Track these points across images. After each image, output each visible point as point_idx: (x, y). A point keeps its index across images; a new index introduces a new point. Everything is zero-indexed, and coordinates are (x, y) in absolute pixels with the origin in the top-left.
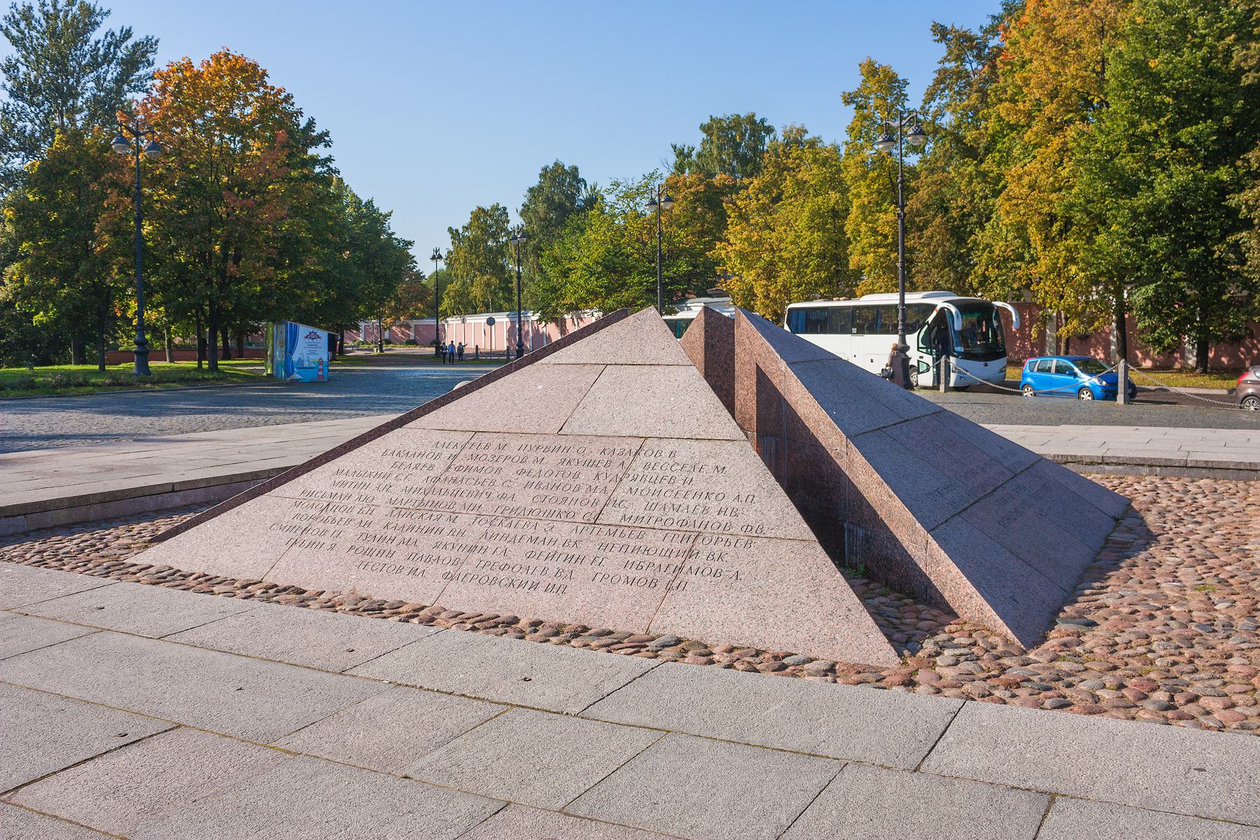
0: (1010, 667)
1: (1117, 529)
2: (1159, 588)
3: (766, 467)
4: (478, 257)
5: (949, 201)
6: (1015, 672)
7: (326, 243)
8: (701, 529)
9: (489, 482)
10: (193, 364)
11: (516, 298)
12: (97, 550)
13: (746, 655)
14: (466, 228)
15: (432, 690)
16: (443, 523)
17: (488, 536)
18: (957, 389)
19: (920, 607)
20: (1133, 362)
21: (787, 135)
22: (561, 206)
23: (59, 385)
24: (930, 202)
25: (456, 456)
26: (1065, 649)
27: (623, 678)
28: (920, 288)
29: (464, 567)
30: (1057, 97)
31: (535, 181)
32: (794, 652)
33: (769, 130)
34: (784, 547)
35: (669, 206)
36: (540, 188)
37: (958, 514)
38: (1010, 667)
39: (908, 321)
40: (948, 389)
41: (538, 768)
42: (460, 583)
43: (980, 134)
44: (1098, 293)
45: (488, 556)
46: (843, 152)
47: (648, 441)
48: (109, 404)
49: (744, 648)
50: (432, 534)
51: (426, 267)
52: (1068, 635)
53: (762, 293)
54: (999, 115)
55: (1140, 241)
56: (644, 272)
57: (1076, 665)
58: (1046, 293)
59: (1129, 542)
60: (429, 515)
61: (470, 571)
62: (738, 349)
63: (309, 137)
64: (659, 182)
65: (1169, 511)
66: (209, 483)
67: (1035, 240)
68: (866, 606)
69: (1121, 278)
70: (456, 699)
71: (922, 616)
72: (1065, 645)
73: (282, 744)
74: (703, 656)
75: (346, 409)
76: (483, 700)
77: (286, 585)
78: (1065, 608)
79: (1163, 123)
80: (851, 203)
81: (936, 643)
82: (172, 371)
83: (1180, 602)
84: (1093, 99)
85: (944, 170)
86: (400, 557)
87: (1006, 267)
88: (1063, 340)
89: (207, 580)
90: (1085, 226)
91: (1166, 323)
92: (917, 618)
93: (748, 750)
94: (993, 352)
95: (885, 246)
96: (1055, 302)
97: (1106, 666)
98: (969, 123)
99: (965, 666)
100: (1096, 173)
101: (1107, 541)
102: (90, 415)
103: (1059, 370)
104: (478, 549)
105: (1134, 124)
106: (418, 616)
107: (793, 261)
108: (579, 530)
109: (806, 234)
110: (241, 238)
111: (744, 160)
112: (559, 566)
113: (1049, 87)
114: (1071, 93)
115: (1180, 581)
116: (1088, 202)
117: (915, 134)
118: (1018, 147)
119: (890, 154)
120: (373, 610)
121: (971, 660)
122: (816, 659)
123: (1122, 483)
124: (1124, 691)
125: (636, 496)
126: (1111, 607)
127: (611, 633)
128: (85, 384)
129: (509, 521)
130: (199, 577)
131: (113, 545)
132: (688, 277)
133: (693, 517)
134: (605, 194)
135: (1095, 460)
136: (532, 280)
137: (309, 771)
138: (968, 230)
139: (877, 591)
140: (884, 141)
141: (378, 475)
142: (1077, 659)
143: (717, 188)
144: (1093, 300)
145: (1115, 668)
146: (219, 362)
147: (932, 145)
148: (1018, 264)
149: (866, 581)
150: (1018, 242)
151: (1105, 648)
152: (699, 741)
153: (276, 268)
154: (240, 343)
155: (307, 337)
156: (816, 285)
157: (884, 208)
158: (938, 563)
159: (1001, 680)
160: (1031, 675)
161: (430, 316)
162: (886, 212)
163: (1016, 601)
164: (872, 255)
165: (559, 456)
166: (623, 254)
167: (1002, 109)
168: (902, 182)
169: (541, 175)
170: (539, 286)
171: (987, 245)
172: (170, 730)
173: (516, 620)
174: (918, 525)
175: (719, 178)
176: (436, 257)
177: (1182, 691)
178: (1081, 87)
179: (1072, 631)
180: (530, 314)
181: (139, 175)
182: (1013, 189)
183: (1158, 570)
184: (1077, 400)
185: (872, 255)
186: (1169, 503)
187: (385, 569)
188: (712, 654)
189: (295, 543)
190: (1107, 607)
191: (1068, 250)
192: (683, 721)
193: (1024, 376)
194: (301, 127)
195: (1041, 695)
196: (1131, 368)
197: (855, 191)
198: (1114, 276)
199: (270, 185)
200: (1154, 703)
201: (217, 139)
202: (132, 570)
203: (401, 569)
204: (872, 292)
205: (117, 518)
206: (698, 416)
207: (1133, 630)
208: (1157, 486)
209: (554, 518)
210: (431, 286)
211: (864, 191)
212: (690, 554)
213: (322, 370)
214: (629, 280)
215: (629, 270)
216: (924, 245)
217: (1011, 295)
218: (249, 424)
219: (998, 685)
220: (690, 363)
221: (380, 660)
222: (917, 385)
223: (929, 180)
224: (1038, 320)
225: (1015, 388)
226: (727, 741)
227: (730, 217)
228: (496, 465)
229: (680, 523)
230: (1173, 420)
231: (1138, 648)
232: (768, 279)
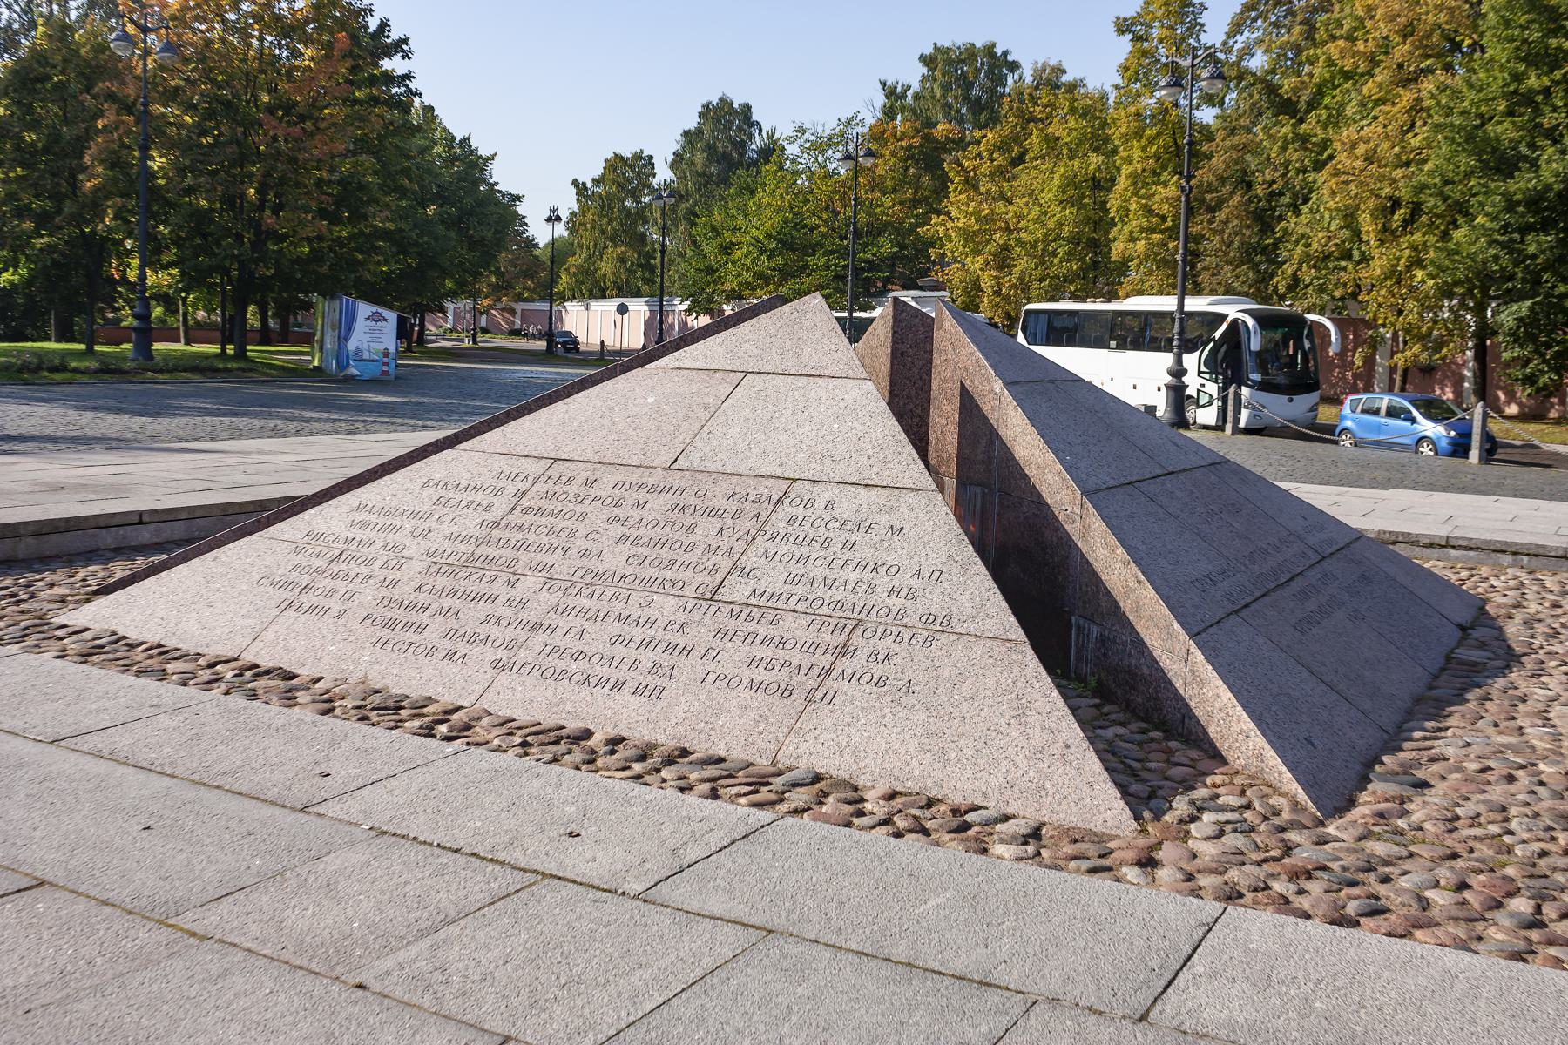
0: (1299, 846)
1: (1465, 642)
2: (1522, 734)
3: (961, 531)
4: (611, 221)
5: (1253, 173)
6: (1306, 854)
7: (402, 192)
8: (863, 616)
9: (567, 531)
10: (214, 349)
11: (658, 280)
12: (17, 603)
13: (912, 805)
14: (596, 182)
15: (431, 844)
16: (499, 588)
17: (560, 609)
18: (1248, 431)
19: (1173, 744)
20: (1494, 406)
21: (1038, 73)
22: (725, 157)
23: (24, 368)
24: (1229, 173)
25: (524, 493)
26: (1382, 821)
27: (717, 839)
28: (1207, 290)
29: (522, 653)
30: (1412, 35)
31: (692, 122)
32: (983, 804)
33: (1014, 66)
34: (979, 649)
35: (869, 162)
36: (699, 132)
37: (1237, 612)
38: (1299, 846)
39: (1189, 336)
40: (1237, 430)
41: (563, 982)
42: (515, 676)
43: (1302, 83)
44: (1451, 309)
45: (557, 639)
46: (1111, 102)
47: (796, 485)
48: (89, 397)
49: (910, 794)
50: (481, 603)
51: (541, 233)
52: (1387, 800)
53: (992, 287)
54: (1329, 59)
55: (1515, 241)
56: (833, 252)
57: (1396, 848)
58: (1380, 305)
59: (1478, 663)
60: (480, 575)
61: (530, 660)
62: (937, 360)
63: (383, 44)
64: (859, 129)
65: (1540, 621)
66: (192, 514)
67: (1368, 232)
68: (1091, 742)
69: (1484, 290)
70: (462, 860)
71: (1174, 759)
72: (1381, 815)
73: (186, 922)
74: (849, 803)
75: (412, 418)
76: (502, 863)
77: (271, 665)
78: (1385, 759)
79: (1558, 77)
80: (1118, 169)
81: (1192, 802)
82: (186, 356)
83: (1553, 757)
84: (1463, 41)
85: (1249, 131)
86: (436, 629)
87: (1327, 267)
88: (1399, 372)
89: (161, 654)
90: (1438, 216)
91: (1543, 355)
92: (1168, 761)
93: (887, 970)
94: (1301, 383)
95: (1161, 232)
96: (1391, 319)
97: (1440, 851)
98: (1287, 68)
99: (1232, 841)
100: (1459, 144)
101: (1448, 659)
102: (61, 411)
103: (1392, 413)
104: (544, 628)
105: (1518, 78)
106: (447, 721)
107: (1034, 246)
108: (688, 609)
109: (1055, 209)
110: (283, 181)
111: (977, 106)
112: (656, 658)
113: (1403, 20)
114: (1433, 31)
115: (1553, 726)
116: (1447, 183)
117: (1212, 77)
118: (1353, 103)
119: (1176, 105)
120: (386, 709)
121: (1242, 832)
122: (1014, 817)
123: (1472, 576)
124: (1467, 895)
125: (773, 563)
126: (1452, 761)
127: (721, 760)
128: (62, 368)
129: (590, 590)
130: (151, 648)
131: (43, 595)
132: (893, 260)
133: (852, 598)
134: (785, 143)
135: (1437, 541)
136: (682, 255)
137: (214, 969)
138: (1277, 214)
139: (1113, 717)
140: (1168, 86)
141: (415, 515)
142: (1398, 838)
143: (937, 140)
144: (1443, 319)
145: (1454, 856)
146: (249, 347)
147: (1234, 95)
148: (1343, 263)
149: (1097, 701)
150: (1346, 233)
151: (1440, 824)
152: (816, 948)
153: (331, 223)
154: (285, 324)
155: (368, 319)
156: (1065, 281)
157: (1163, 179)
158: (1202, 683)
159: (1284, 866)
160: (1329, 860)
161: (542, 299)
162: (1166, 185)
163: (1312, 744)
164: (1143, 242)
165: (670, 499)
166: (806, 226)
167: (1333, 49)
168: (1191, 143)
169: (701, 115)
170: (690, 264)
171: (1303, 236)
172: (25, 889)
173: (588, 734)
174: (1177, 626)
175: (942, 129)
176: (553, 219)
177: (1555, 899)
178: (1447, 23)
179: (1393, 794)
180: (677, 301)
181: (146, 87)
182: (1343, 160)
183: (1521, 707)
184: (1414, 456)
185: (1143, 242)
186: (1540, 608)
187: (411, 649)
188: (862, 800)
189: (290, 605)
190: (1446, 759)
191: (1414, 248)
192: (795, 916)
193: (1343, 418)
194: (370, 30)
195: (1342, 894)
196: (1492, 414)
197: (1125, 154)
198: (1475, 287)
199: (326, 108)
200: (1512, 915)
201: (255, 42)
202: (60, 633)
203: (434, 649)
204: (1141, 293)
205: (58, 556)
206: (870, 452)
207: (1482, 797)
208: (1522, 583)
209: (654, 588)
210: (545, 257)
211: (1137, 154)
212: (844, 650)
213: (387, 364)
214: (811, 261)
215: (814, 248)
216: (1215, 232)
217: (1331, 306)
218: (276, 433)
219: (1279, 874)
220: (864, 375)
221: (365, 791)
222: (1195, 423)
223: (1228, 143)
224: (1365, 342)
225: (1327, 434)
226: (857, 952)
227: (952, 182)
228: (579, 509)
229: (832, 606)
230: (1547, 489)
231: (1490, 827)
232: (1000, 268)
